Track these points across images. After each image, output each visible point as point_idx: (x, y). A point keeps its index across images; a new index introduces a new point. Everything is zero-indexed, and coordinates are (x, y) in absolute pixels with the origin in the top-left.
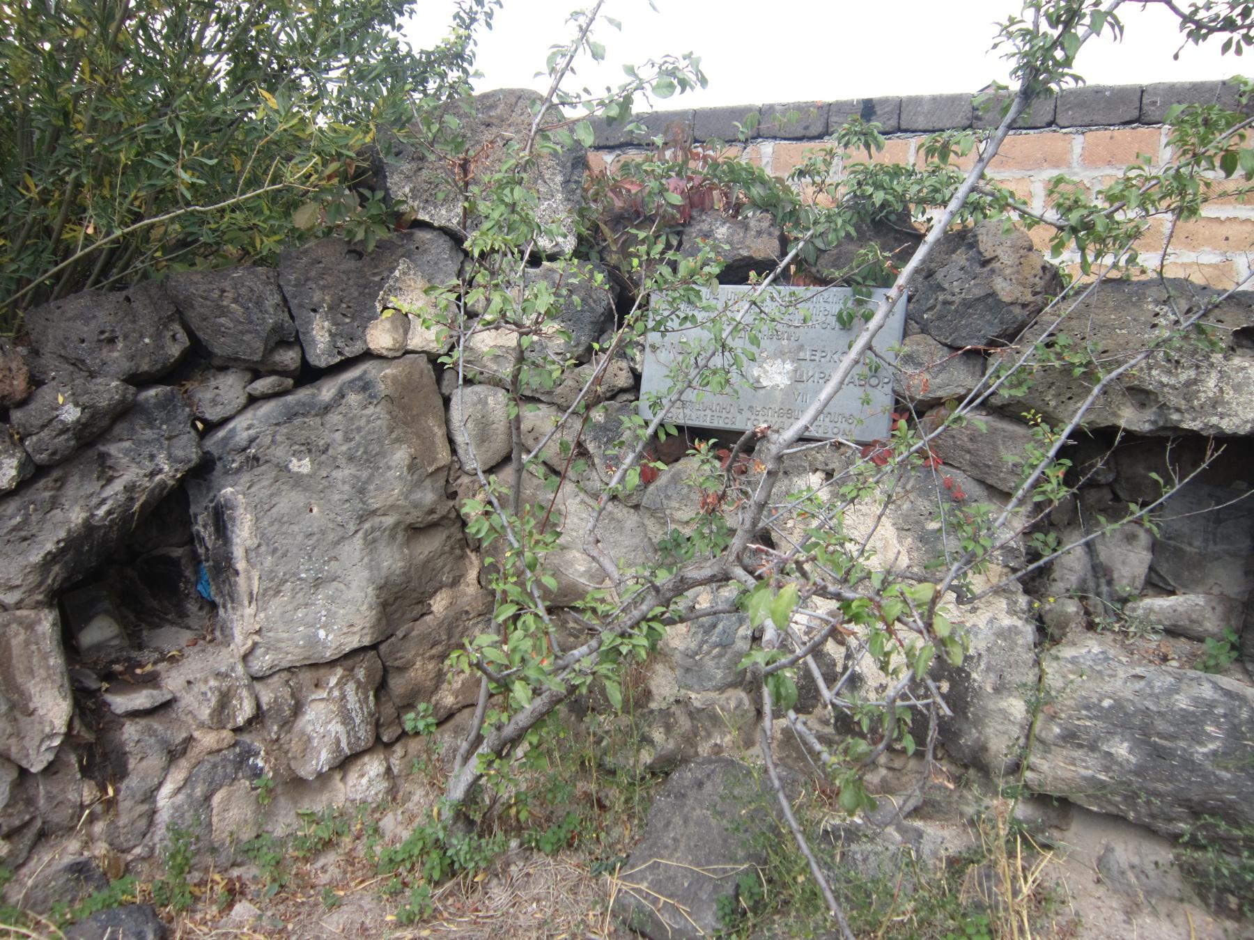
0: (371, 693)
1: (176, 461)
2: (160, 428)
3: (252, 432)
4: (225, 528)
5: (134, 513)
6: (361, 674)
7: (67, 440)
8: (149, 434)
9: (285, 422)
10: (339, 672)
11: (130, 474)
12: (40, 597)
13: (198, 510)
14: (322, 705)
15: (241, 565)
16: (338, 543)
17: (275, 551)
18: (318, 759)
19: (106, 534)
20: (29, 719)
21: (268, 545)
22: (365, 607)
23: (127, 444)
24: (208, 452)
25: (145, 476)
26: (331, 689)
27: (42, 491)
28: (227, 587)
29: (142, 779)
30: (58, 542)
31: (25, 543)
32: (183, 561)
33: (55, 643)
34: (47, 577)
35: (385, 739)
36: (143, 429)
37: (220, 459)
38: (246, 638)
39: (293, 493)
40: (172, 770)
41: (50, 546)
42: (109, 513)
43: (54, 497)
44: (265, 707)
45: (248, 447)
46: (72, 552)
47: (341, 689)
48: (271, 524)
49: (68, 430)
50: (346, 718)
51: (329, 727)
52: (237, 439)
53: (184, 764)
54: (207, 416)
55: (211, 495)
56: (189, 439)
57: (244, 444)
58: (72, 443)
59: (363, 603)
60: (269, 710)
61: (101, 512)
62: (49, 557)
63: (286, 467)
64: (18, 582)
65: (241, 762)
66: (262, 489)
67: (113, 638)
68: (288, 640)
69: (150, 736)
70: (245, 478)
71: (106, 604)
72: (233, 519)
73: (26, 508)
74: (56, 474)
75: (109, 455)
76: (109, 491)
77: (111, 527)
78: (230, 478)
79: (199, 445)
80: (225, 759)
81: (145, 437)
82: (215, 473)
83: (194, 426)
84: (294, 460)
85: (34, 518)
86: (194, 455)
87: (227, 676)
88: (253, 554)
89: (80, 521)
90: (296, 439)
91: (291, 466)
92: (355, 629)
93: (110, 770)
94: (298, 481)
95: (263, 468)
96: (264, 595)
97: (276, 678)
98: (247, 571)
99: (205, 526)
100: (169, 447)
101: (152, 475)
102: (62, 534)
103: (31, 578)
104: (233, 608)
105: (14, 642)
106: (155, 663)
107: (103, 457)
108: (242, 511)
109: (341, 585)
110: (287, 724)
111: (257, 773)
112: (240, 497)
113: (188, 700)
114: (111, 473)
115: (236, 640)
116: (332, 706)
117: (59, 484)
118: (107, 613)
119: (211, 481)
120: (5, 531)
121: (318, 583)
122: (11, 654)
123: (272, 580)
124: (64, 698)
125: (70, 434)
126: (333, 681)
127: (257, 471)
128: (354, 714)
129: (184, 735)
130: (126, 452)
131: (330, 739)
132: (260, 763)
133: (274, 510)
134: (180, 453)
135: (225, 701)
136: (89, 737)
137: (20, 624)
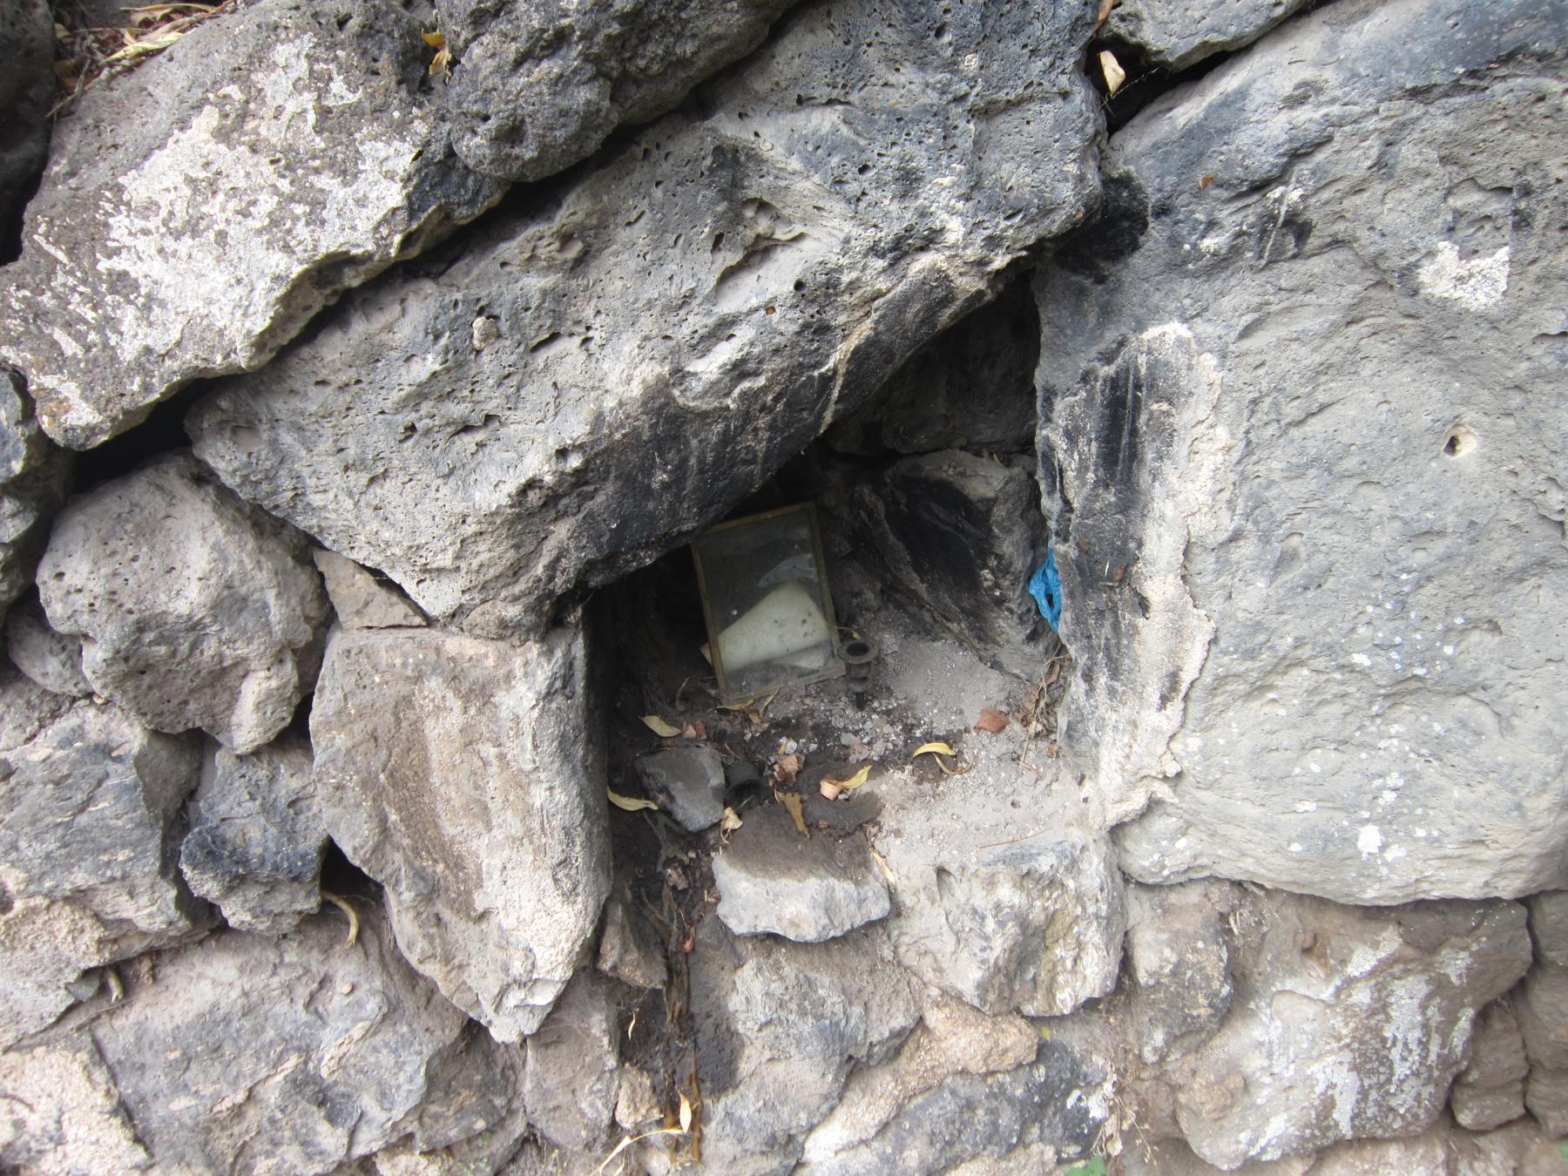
0: (1469, 1013)
1: (994, 208)
2: (951, 66)
3: (1307, 116)
4: (1134, 456)
5: (827, 380)
6: (1455, 965)
7: (561, 83)
8: (908, 86)
9: (1456, 87)
10: (1390, 941)
11: (823, 239)
12: (513, 612)
13: (1060, 380)
14: (1310, 1010)
15: (1159, 586)
16: (1519, 576)
17: (1285, 560)
18: (1258, 1133)
19: (726, 438)
20: (474, 930)
21: (1265, 539)
22: (1545, 801)
23: (824, 121)
24: (1125, 181)
25: (874, 250)
26: (1350, 982)
27: (518, 271)
28: (1106, 631)
29: (769, 1107)
30: (562, 453)
31: (469, 441)
32: (999, 512)
33: (549, 747)
34: (536, 552)
35: (1465, 1118)
36: (894, 64)
37: (1163, 211)
38: (1132, 786)
39: (1405, 375)
40: (853, 1095)
41: (537, 464)
42: (739, 370)
43: (558, 297)
44: (1143, 978)
45: (1279, 177)
46: (610, 488)
47: (1380, 987)
48: (1296, 472)
49: (561, 39)
50: (1370, 1057)
51: (1315, 1068)
52: (1243, 139)
53: (885, 1084)
54: (1150, 36)
55: (1111, 335)
56: (1059, 125)
57: (1265, 162)
58: (583, 95)
59: (1544, 787)
60: (1154, 988)
61: (710, 366)
62: (534, 497)
63: (1407, 273)
64: (446, 560)
65: (1042, 1106)
66: (1289, 348)
67: (806, 650)
68: (1256, 825)
69: (803, 1013)
70: (1240, 294)
71: (805, 564)
72: (1167, 435)
73: (460, 325)
74: (573, 210)
75: (757, 159)
76: (745, 294)
77: (747, 417)
78: (1185, 287)
79: (1099, 146)
80: (1000, 1093)
81: (893, 98)
82: (1137, 260)
83: (1091, 70)
84: (1448, 252)
85: (488, 364)
86: (1066, 188)
87: (1053, 883)
88: (1205, 562)
89: (636, 390)
90: (1482, 164)
91: (1425, 274)
92: (1486, 854)
93: (689, 1064)
94: (1437, 334)
95: (1316, 265)
96: (1213, 691)
97: (1193, 895)
98: (1171, 608)
99: (1071, 436)
100: (979, 145)
101: (900, 250)
102: (576, 428)
103: (483, 552)
104: (1112, 692)
105: (433, 730)
106: (880, 767)
107: (732, 162)
108: (1203, 411)
109: (1484, 716)
110: (1190, 1036)
111: (1083, 1134)
112: (1210, 360)
113: (928, 923)
114: (763, 225)
115: (1103, 779)
116: (1337, 1022)
117: (575, 249)
118: (806, 585)
119: (1118, 288)
120: (395, 396)
121: (1402, 690)
122: (426, 759)
123: (1251, 654)
124: (569, 896)
125: (571, 57)
126: (1362, 961)
127: (1290, 273)
128: (1395, 1054)
129: (899, 1021)
130: (817, 151)
131: (1305, 1100)
132: (1096, 1110)
133: (1315, 425)
134: (1016, 176)
135: (1031, 944)
136: (641, 973)
137: (454, 679)
